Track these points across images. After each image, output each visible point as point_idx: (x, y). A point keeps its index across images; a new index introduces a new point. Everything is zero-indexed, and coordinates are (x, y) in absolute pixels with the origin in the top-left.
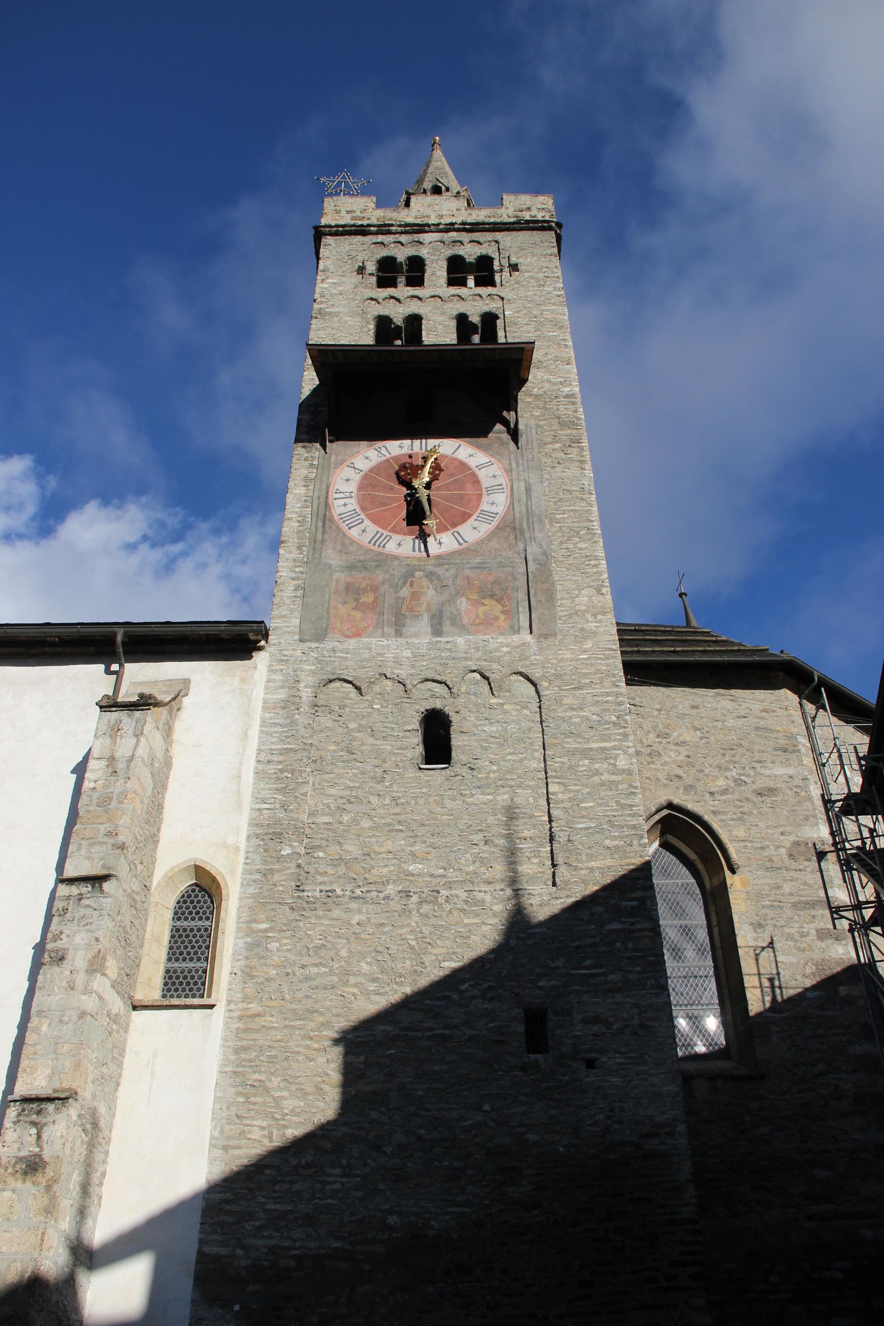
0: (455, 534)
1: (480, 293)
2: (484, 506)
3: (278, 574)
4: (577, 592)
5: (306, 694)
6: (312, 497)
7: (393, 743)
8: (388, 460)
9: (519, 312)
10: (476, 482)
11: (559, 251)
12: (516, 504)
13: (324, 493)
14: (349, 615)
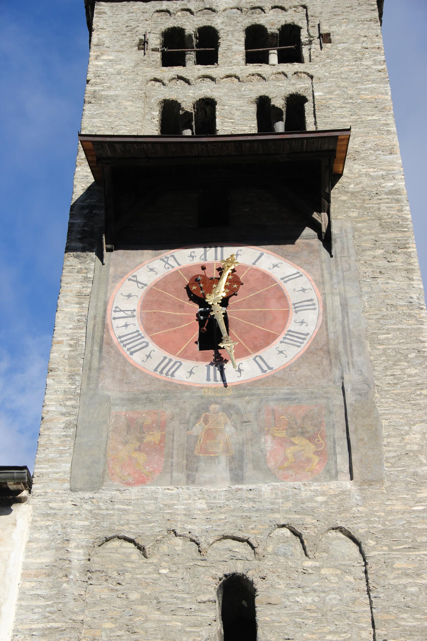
0: (258, 359)
1: (285, 71)
2: (292, 326)
3: (45, 408)
4: (407, 428)
5: (77, 556)
7: (184, 618)
8: (177, 272)
9: (331, 93)
10: (282, 296)
11: (381, 15)
12: (330, 323)
14: (130, 458)
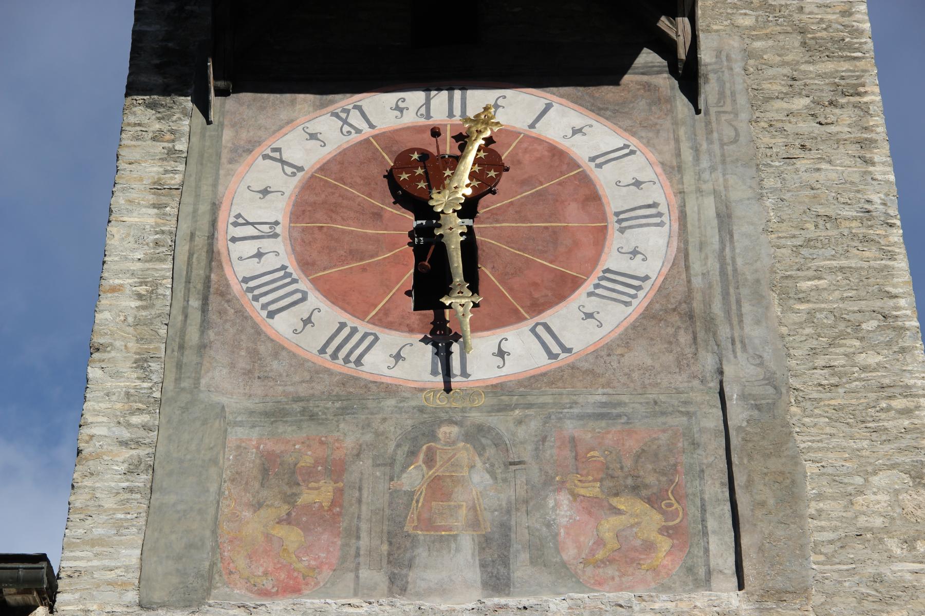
0: (540, 330)
2: (612, 260)
3: (85, 431)
4: (859, 480)
6: (174, 234)
8: (367, 141)
10: (592, 198)
12: (694, 254)
13: (204, 223)
14: (268, 537)
